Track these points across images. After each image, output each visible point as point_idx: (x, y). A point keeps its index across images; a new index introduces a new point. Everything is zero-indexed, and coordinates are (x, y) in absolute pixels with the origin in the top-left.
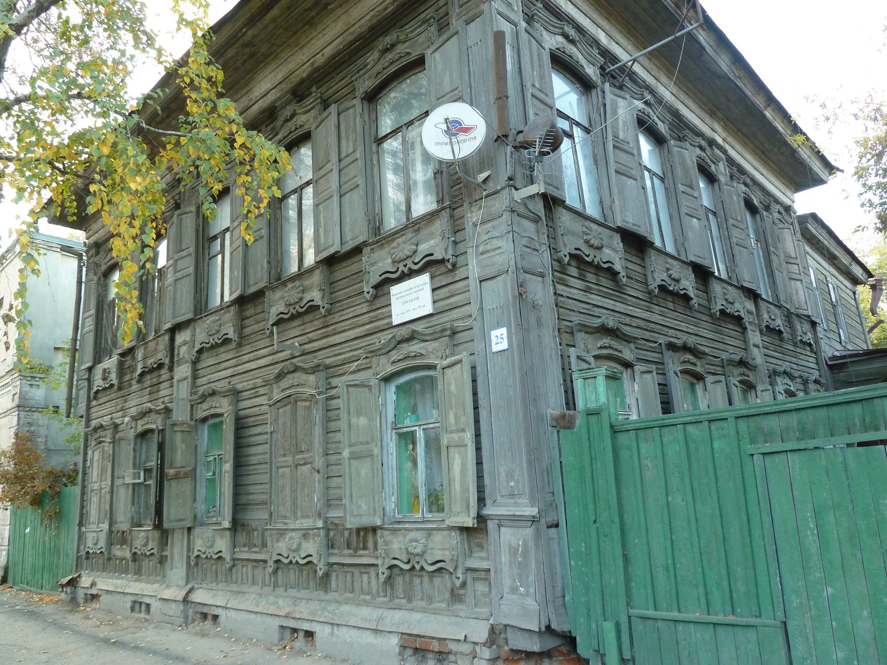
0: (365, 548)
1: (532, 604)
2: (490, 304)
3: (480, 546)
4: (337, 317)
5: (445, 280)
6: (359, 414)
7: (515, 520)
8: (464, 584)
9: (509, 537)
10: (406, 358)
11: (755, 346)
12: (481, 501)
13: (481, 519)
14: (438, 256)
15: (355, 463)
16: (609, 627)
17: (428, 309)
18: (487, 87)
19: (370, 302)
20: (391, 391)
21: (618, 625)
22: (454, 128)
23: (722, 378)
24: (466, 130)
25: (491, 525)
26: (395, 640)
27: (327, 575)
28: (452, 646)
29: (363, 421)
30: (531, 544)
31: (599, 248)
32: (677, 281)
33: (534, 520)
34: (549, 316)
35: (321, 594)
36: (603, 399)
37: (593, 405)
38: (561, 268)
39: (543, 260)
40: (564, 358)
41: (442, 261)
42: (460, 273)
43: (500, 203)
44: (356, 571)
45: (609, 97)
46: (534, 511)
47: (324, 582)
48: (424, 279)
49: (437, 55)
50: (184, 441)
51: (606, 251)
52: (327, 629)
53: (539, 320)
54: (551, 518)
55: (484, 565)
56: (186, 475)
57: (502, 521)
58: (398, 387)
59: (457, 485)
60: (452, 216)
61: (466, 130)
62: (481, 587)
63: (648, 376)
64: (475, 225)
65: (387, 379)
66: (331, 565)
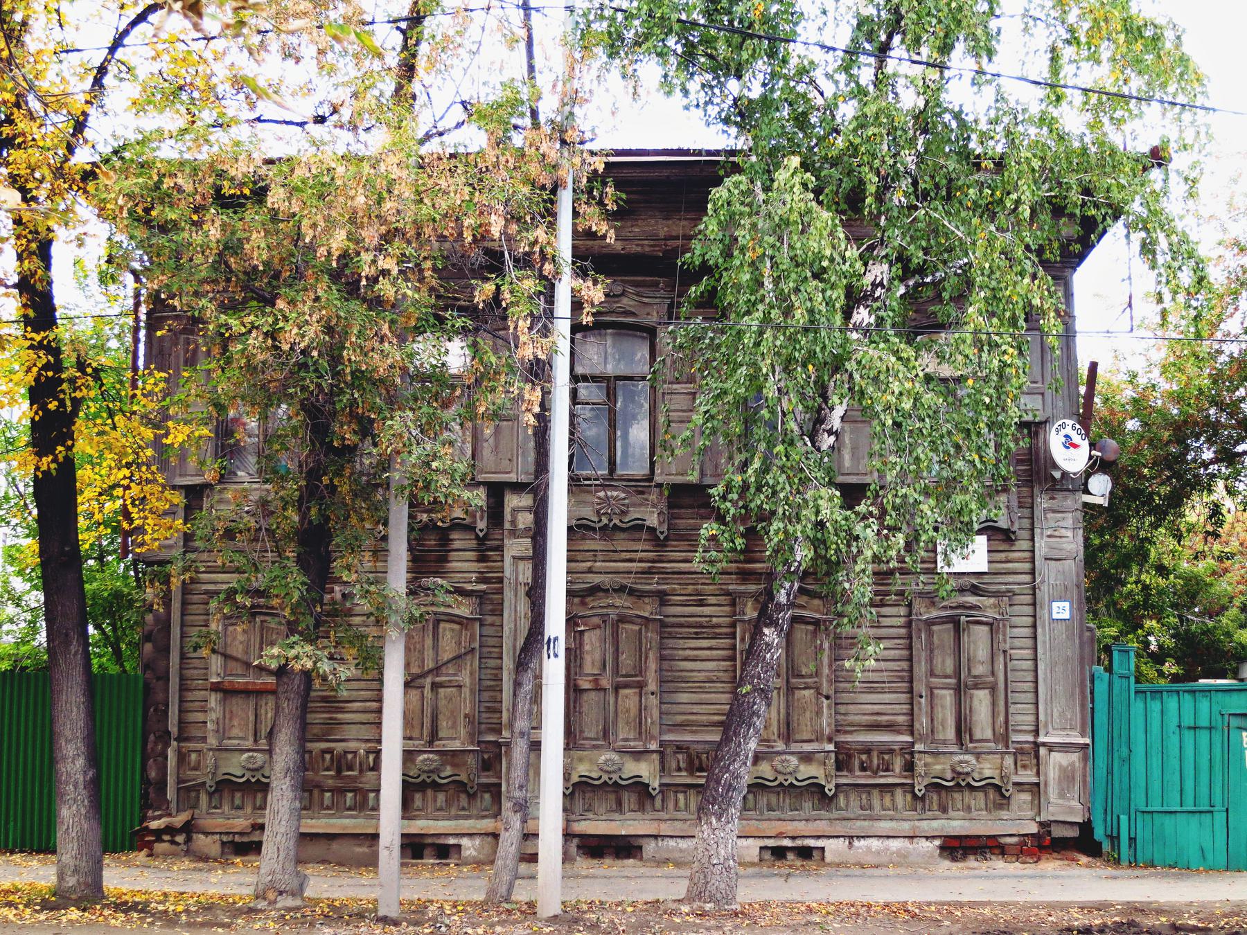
7: (1066, 747)
9: (1058, 760)
17: (984, 568)
52: (841, 844)
57: (1051, 747)
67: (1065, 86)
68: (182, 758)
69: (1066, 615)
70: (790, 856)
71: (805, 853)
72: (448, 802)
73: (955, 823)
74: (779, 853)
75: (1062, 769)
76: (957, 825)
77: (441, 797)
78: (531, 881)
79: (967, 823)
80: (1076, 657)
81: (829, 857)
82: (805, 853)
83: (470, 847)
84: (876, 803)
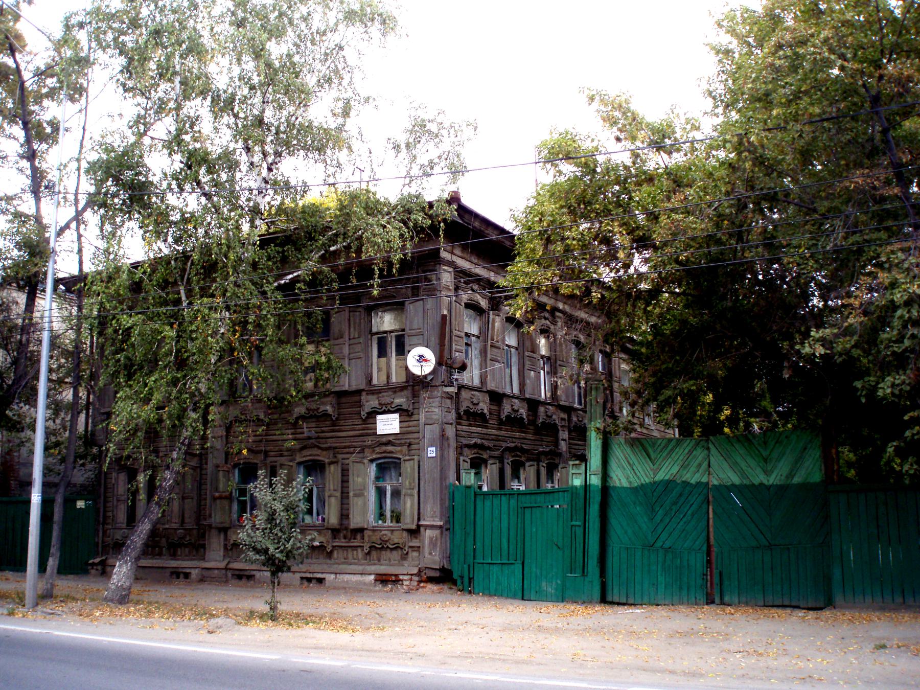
0: (355, 539)
1: (437, 558)
2: (427, 436)
3: (416, 538)
4: (342, 423)
5: (407, 419)
6: (358, 476)
7: (432, 527)
8: (407, 553)
9: (428, 534)
10: (385, 452)
11: (563, 440)
12: (419, 519)
13: (419, 526)
14: (404, 407)
15: (356, 499)
16: (466, 566)
17: (397, 431)
18: (434, 340)
19: (364, 420)
20: (373, 467)
21: (469, 566)
22: (422, 359)
23: (535, 463)
24: (426, 361)
25: (422, 529)
26: (372, 577)
27: (332, 552)
28: (401, 577)
29: (360, 480)
30: (439, 536)
31: (477, 404)
32: (517, 411)
33: (441, 527)
34: (453, 443)
35: (328, 561)
36: (472, 482)
37: (468, 484)
38: (459, 417)
39: (452, 416)
40: (458, 460)
41: (407, 411)
42: (415, 417)
43: (438, 393)
44: (350, 550)
45: (491, 317)
46: (441, 523)
47: (330, 555)
48: (397, 415)
49: (411, 306)
50: (224, 477)
51: (481, 404)
52: (333, 576)
53: (449, 445)
54: (448, 526)
55: (418, 545)
56: (226, 498)
57: (427, 527)
58: (377, 465)
59: (408, 511)
60: (413, 389)
61: (426, 361)
62: (415, 554)
63: (494, 466)
64: (425, 398)
65: (372, 461)
66: (334, 547)
67: (690, 452)
68: (104, 532)
69: (434, 455)
70: (314, 581)
71: (320, 581)
72: (190, 552)
73: (383, 567)
74: (309, 580)
75: (431, 539)
76: (383, 569)
77: (187, 550)
78: (597, 594)
79: (388, 567)
80: (439, 477)
81: (327, 584)
82: (320, 581)
83: (194, 573)
84: (350, 556)
